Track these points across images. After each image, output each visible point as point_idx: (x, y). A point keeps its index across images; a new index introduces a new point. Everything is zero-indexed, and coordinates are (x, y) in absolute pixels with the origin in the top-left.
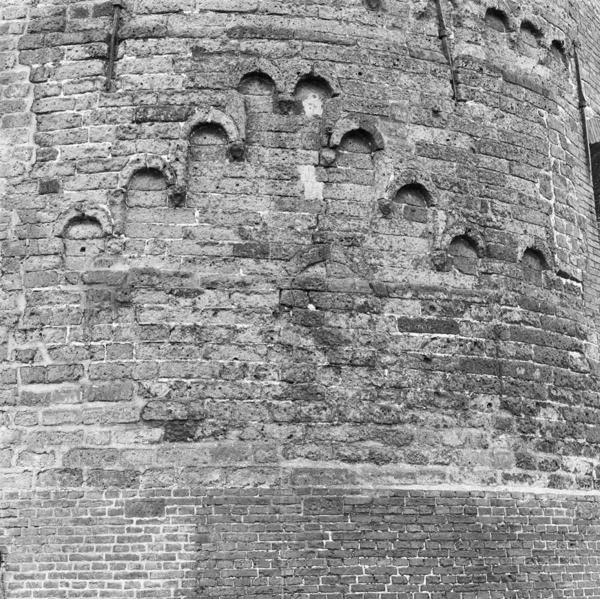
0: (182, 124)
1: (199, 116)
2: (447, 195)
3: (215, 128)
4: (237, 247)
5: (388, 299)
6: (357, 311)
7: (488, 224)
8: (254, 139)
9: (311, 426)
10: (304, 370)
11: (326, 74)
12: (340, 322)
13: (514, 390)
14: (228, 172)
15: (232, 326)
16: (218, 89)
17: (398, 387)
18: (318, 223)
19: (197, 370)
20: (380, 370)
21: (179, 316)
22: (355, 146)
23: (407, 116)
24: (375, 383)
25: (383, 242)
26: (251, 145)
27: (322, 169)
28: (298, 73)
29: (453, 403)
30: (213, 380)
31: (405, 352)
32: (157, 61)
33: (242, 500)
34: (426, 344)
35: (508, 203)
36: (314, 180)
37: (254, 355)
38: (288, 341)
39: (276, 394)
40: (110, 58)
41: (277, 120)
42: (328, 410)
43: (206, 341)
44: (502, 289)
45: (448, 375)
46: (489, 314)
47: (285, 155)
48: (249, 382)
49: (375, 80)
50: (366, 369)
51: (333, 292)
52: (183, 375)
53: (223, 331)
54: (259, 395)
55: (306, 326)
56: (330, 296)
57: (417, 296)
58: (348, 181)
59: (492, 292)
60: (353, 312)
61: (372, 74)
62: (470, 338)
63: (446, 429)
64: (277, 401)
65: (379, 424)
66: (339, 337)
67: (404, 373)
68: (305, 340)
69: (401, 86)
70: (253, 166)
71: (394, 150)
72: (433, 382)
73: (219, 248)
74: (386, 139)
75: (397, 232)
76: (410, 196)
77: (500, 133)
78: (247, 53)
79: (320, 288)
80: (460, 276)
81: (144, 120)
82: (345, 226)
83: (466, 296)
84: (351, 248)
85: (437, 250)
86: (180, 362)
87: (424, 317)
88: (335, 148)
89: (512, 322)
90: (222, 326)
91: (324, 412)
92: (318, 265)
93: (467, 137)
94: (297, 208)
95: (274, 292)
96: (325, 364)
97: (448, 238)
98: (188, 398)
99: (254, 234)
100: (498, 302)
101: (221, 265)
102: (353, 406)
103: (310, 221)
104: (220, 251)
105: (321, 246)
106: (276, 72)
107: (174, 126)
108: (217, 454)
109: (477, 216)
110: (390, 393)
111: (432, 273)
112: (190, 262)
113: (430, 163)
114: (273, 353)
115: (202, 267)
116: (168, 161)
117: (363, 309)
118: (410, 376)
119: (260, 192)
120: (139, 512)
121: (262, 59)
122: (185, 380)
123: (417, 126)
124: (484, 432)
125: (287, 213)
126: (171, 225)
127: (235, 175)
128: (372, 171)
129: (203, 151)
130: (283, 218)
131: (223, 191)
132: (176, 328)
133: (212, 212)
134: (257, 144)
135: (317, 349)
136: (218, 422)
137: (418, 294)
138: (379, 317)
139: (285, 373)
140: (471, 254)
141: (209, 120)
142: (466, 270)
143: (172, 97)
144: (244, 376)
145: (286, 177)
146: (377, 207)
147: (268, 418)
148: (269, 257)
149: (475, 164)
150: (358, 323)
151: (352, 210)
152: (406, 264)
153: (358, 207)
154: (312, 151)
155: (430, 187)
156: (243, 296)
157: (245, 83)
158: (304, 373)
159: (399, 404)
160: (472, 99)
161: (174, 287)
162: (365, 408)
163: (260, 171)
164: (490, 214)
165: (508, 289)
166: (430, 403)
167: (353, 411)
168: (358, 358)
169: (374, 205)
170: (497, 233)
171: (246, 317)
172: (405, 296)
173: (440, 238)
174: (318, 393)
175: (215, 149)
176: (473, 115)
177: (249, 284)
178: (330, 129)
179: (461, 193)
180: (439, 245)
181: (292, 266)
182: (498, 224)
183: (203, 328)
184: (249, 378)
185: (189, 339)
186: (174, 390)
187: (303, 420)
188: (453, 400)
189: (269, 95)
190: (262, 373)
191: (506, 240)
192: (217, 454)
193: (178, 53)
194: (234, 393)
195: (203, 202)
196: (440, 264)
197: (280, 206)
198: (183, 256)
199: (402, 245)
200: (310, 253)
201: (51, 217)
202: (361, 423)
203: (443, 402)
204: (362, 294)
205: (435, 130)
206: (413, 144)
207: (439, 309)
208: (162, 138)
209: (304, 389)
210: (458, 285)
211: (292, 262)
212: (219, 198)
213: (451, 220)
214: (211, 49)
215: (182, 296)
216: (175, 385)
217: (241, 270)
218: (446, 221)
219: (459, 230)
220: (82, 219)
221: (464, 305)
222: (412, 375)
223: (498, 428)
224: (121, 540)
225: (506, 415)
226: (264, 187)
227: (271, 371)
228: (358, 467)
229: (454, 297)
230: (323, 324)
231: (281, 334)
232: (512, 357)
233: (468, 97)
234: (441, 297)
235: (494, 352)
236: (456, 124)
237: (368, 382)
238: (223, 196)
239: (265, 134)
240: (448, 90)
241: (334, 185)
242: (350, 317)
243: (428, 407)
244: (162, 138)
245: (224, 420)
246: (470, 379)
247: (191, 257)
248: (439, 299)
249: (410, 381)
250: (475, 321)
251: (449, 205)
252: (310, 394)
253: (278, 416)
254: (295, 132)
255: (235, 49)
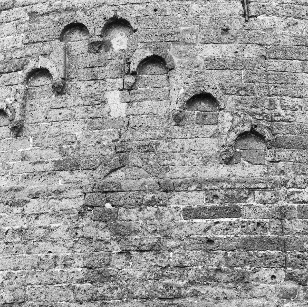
0: (20, 73)
1: (32, 65)
2: (233, 99)
3: (44, 72)
4: (57, 163)
5: (174, 193)
6: (145, 205)
7: (276, 118)
8: (73, 76)
9: (105, 304)
10: (100, 258)
11: (126, 16)
13: (301, 262)
14: (54, 105)
15: (47, 226)
16: (45, 41)
17: (181, 266)
18: (120, 136)
19: (22, 263)
20: (165, 253)
21: (12, 221)
22: (153, 69)
23: (196, 38)
24: (159, 264)
25: (176, 145)
26: (70, 81)
27: (127, 92)
28: (105, 18)
29: (232, 277)
30: (33, 270)
31: (188, 236)
32: (7, 27)
34: (209, 228)
35: (299, 98)
36: (118, 102)
37: (63, 248)
38: (89, 235)
39: (78, 278)
41: (92, 58)
42: (119, 289)
43: (30, 240)
44: (289, 174)
45: (229, 253)
46: (274, 197)
47: (97, 84)
48: (59, 270)
49: (168, 13)
50: (152, 253)
51: (126, 191)
52: (12, 268)
53: (41, 231)
54: (66, 280)
55: (103, 221)
56: (123, 195)
57: (201, 188)
58: (146, 99)
59: (278, 178)
60: (143, 206)
61: (165, 8)
62: (253, 220)
63: (225, 301)
64: (79, 284)
65: (163, 299)
66: (129, 228)
67: (186, 254)
68: (103, 233)
69: (192, 14)
70: (72, 98)
71: (183, 68)
72: (215, 260)
73: (45, 165)
74: (176, 60)
75: (189, 136)
76: (203, 104)
77: (292, 38)
79: (114, 189)
80: (249, 166)
82: (144, 136)
83: (250, 183)
84: (148, 154)
85: (223, 146)
86: (11, 258)
87: (207, 205)
88: (134, 74)
89: (300, 202)
90: (40, 227)
91: (116, 291)
92: (119, 170)
93: (257, 47)
94: (105, 126)
95: (81, 196)
96: (118, 251)
97: (234, 135)
98: (15, 286)
99: (70, 151)
100: (285, 185)
101: (46, 178)
102: (140, 284)
103: (114, 135)
104: (45, 168)
105: (122, 155)
106: (88, 20)
107: (15, 75)
109: (264, 113)
110: (174, 272)
111: (221, 166)
112: (25, 178)
113: (217, 74)
114: (78, 245)
115: (34, 181)
116: (10, 102)
117: (151, 203)
118: (192, 256)
119: (76, 117)
121: (78, 12)
122: (13, 272)
123: (206, 45)
124: (267, 302)
125: (97, 131)
126: (14, 151)
127: (58, 107)
128: (168, 88)
129: (37, 91)
130: (93, 136)
131: (50, 120)
132: (9, 231)
133: (41, 138)
134: (75, 80)
135: (112, 239)
136: (36, 303)
137: (201, 186)
138: (165, 209)
139: (85, 261)
140: (261, 146)
141: (39, 67)
142: (254, 161)
143: (15, 53)
144: (56, 266)
145: (97, 102)
146: (171, 117)
147: (73, 298)
148: (80, 168)
149: (264, 69)
150: (147, 215)
151: (149, 122)
152: (196, 161)
153: (155, 119)
154: (118, 79)
155: (217, 94)
156: (57, 201)
157: (69, 33)
158: (101, 260)
159: (183, 281)
160: (263, 13)
161: (9, 200)
162: (150, 286)
163: (77, 101)
164: (279, 110)
165: (296, 173)
166: (209, 278)
167: (139, 289)
168: (144, 245)
169: (169, 116)
170: (286, 125)
171: (57, 218)
172: (190, 189)
173: (225, 136)
174: (111, 276)
175: (46, 88)
176: (264, 27)
177: (63, 192)
178: (129, 59)
179: (248, 95)
180: (224, 143)
181: (97, 174)
182: (287, 118)
183: (27, 229)
184: (60, 266)
185: (17, 239)
186: (6, 279)
187: (99, 298)
188: (233, 275)
189: (86, 39)
190: (69, 262)
191: (296, 131)
193: (20, 19)
194: (47, 280)
195: (35, 131)
196: (227, 159)
198: (20, 174)
199: (192, 146)
200: (112, 161)
202: (147, 298)
203: (224, 277)
204: (150, 191)
205: (223, 46)
206: (202, 60)
207: (222, 197)
208: (6, 86)
209: (99, 273)
210: (246, 175)
211: (98, 170)
212: (47, 126)
213: (237, 120)
214: (41, 11)
215: (14, 205)
216: (7, 276)
217: (60, 181)
218: (232, 121)
219: (245, 127)
221: (247, 192)
222: (193, 255)
223: (282, 298)
225: (291, 285)
226: (80, 113)
227: (76, 260)
229: (238, 186)
230: (116, 219)
231: (84, 229)
232: (299, 233)
233: (259, 12)
234: (225, 186)
235: (278, 230)
236: (245, 37)
237: (154, 264)
238: (50, 124)
239: (82, 71)
241: (135, 104)
242: (140, 211)
243: (208, 282)
244: (6, 86)
245: (40, 301)
246: (252, 255)
247: (26, 175)
248: (222, 188)
249: (192, 260)
250: (259, 204)
251: (235, 107)
253: (79, 297)
254: (105, 65)
255: (58, 8)
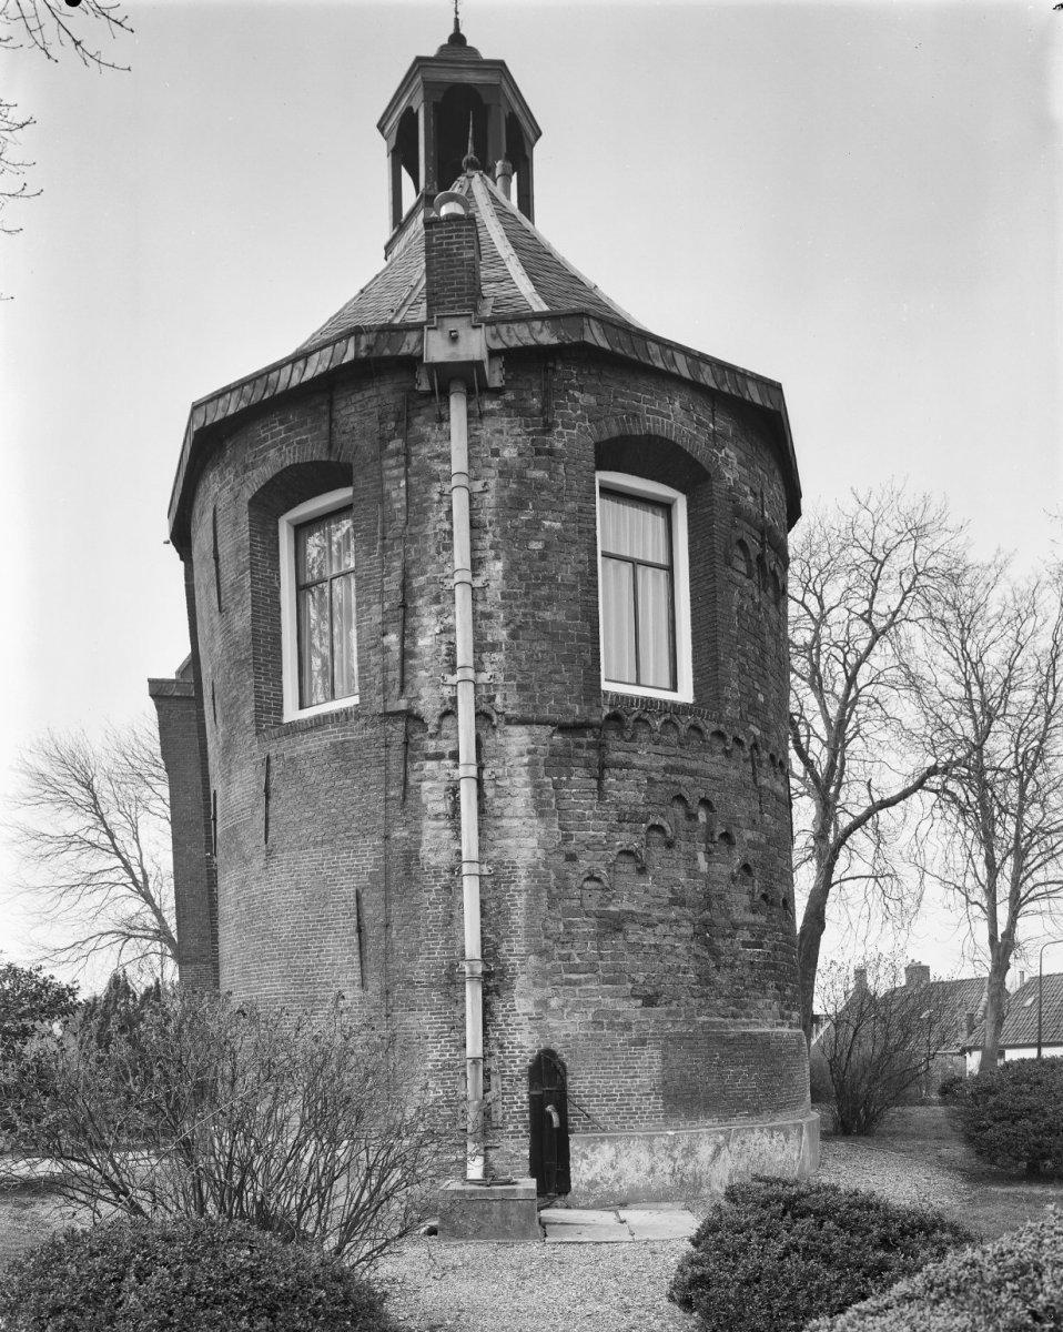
1: (652, 821)
3: (659, 828)
12: (719, 943)
33: (681, 1037)
40: (600, 779)
53: (668, 947)
78: (675, 783)
81: (624, 821)
108: (669, 1013)
120: (634, 1044)
192: (669, 1013)
197: (689, 876)
201: (575, 876)
220: (591, 878)
224: (627, 1059)
228: (727, 1020)
240: (758, 808)
252: (708, 982)
